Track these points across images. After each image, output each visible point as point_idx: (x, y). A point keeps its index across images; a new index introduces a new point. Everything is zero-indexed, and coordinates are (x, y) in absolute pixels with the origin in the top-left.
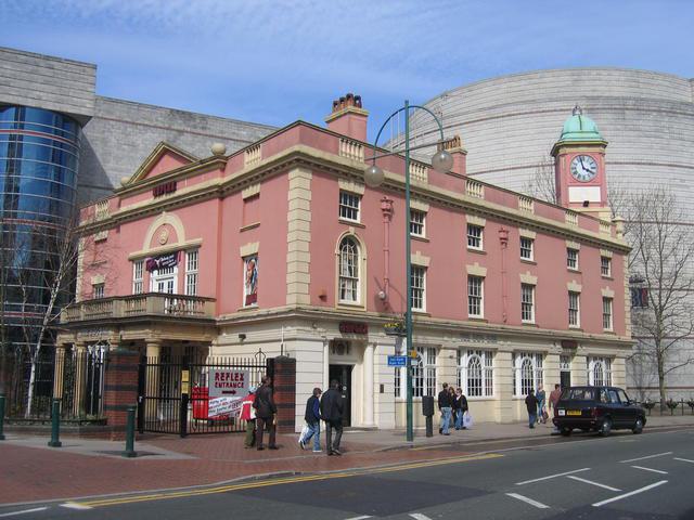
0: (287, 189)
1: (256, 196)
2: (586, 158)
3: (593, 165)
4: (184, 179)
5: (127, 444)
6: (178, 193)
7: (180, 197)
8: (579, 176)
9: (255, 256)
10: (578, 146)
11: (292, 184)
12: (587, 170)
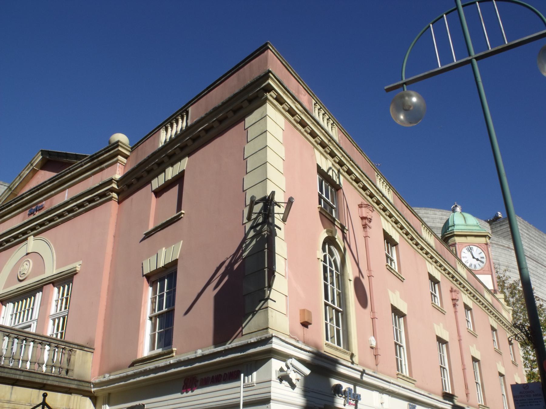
12: (477, 260)
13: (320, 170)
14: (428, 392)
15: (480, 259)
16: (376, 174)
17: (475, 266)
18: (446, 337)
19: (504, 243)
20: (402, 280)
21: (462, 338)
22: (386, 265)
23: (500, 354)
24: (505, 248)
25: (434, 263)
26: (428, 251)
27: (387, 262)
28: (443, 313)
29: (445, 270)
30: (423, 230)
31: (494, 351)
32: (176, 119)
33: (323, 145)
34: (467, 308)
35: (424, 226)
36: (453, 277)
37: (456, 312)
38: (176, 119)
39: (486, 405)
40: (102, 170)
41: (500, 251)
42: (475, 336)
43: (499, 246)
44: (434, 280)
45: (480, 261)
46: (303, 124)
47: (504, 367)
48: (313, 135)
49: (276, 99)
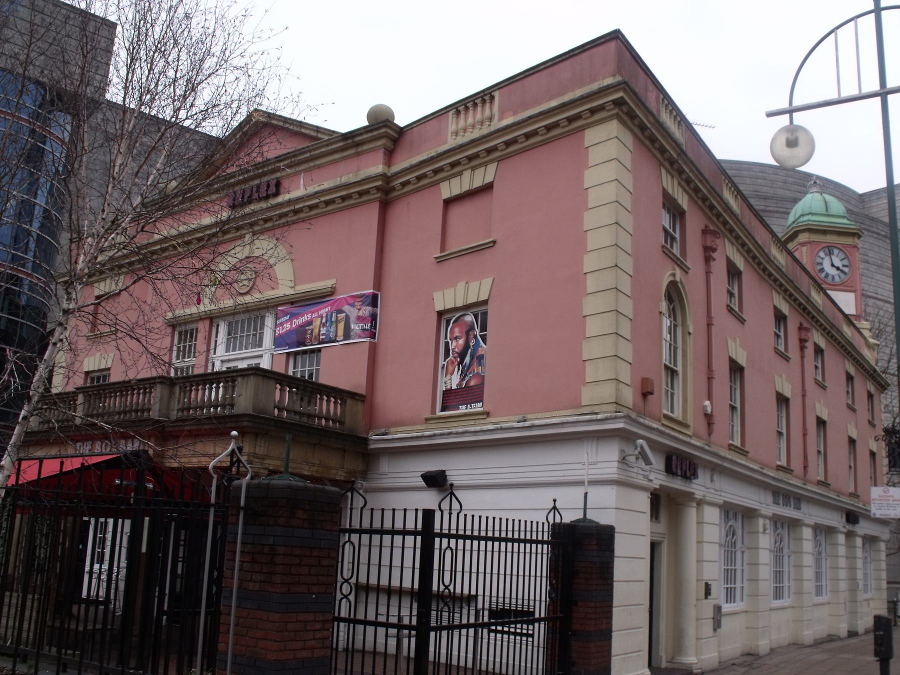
0: (582, 163)
1: (488, 188)
2: (836, 251)
3: (846, 262)
4: (298, 174)
5: (57, 651)
6: (280, 199)
7: (290, 202)
8: (827, 275)
9: (480, 309)
10: (824, 232)
11: (595, 155)
12: (838, 269)
13: (665, 194)
14: (759, 463)
15: (841, 268)
16: (724, 178)
17: (833, 278)
18: (787, 393)
19: (881, 228)
20: (742, 321)
21: (715, 322)
22: (663, 247)
23: (854, 410)
24: (880, 237)
25: (782, 293)
26: (778, 277)
27: (666, 242)
28: (787, 359)
29: (796, 300)
30: (725, 188)
31: (661, 252)
32: (466, 106)
33: (672, 162)
34: (819, 351)
35: (727, 181)
36: (805, 309)
37: (708, 273)
38: (466, 106)
39: (744, 447)
40: (358, 154)
41: (871, 241)
42: (824, 388)
43: (871, 234)
44: (780, 318)
45: (842, 271)
46: (653, 140)
47: (857, 428)
48: (663, 151)
49: (627, 114)
